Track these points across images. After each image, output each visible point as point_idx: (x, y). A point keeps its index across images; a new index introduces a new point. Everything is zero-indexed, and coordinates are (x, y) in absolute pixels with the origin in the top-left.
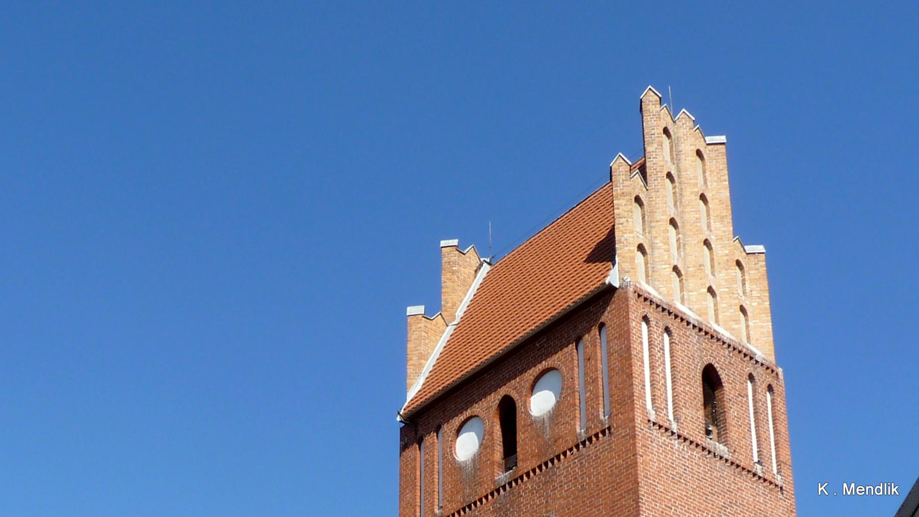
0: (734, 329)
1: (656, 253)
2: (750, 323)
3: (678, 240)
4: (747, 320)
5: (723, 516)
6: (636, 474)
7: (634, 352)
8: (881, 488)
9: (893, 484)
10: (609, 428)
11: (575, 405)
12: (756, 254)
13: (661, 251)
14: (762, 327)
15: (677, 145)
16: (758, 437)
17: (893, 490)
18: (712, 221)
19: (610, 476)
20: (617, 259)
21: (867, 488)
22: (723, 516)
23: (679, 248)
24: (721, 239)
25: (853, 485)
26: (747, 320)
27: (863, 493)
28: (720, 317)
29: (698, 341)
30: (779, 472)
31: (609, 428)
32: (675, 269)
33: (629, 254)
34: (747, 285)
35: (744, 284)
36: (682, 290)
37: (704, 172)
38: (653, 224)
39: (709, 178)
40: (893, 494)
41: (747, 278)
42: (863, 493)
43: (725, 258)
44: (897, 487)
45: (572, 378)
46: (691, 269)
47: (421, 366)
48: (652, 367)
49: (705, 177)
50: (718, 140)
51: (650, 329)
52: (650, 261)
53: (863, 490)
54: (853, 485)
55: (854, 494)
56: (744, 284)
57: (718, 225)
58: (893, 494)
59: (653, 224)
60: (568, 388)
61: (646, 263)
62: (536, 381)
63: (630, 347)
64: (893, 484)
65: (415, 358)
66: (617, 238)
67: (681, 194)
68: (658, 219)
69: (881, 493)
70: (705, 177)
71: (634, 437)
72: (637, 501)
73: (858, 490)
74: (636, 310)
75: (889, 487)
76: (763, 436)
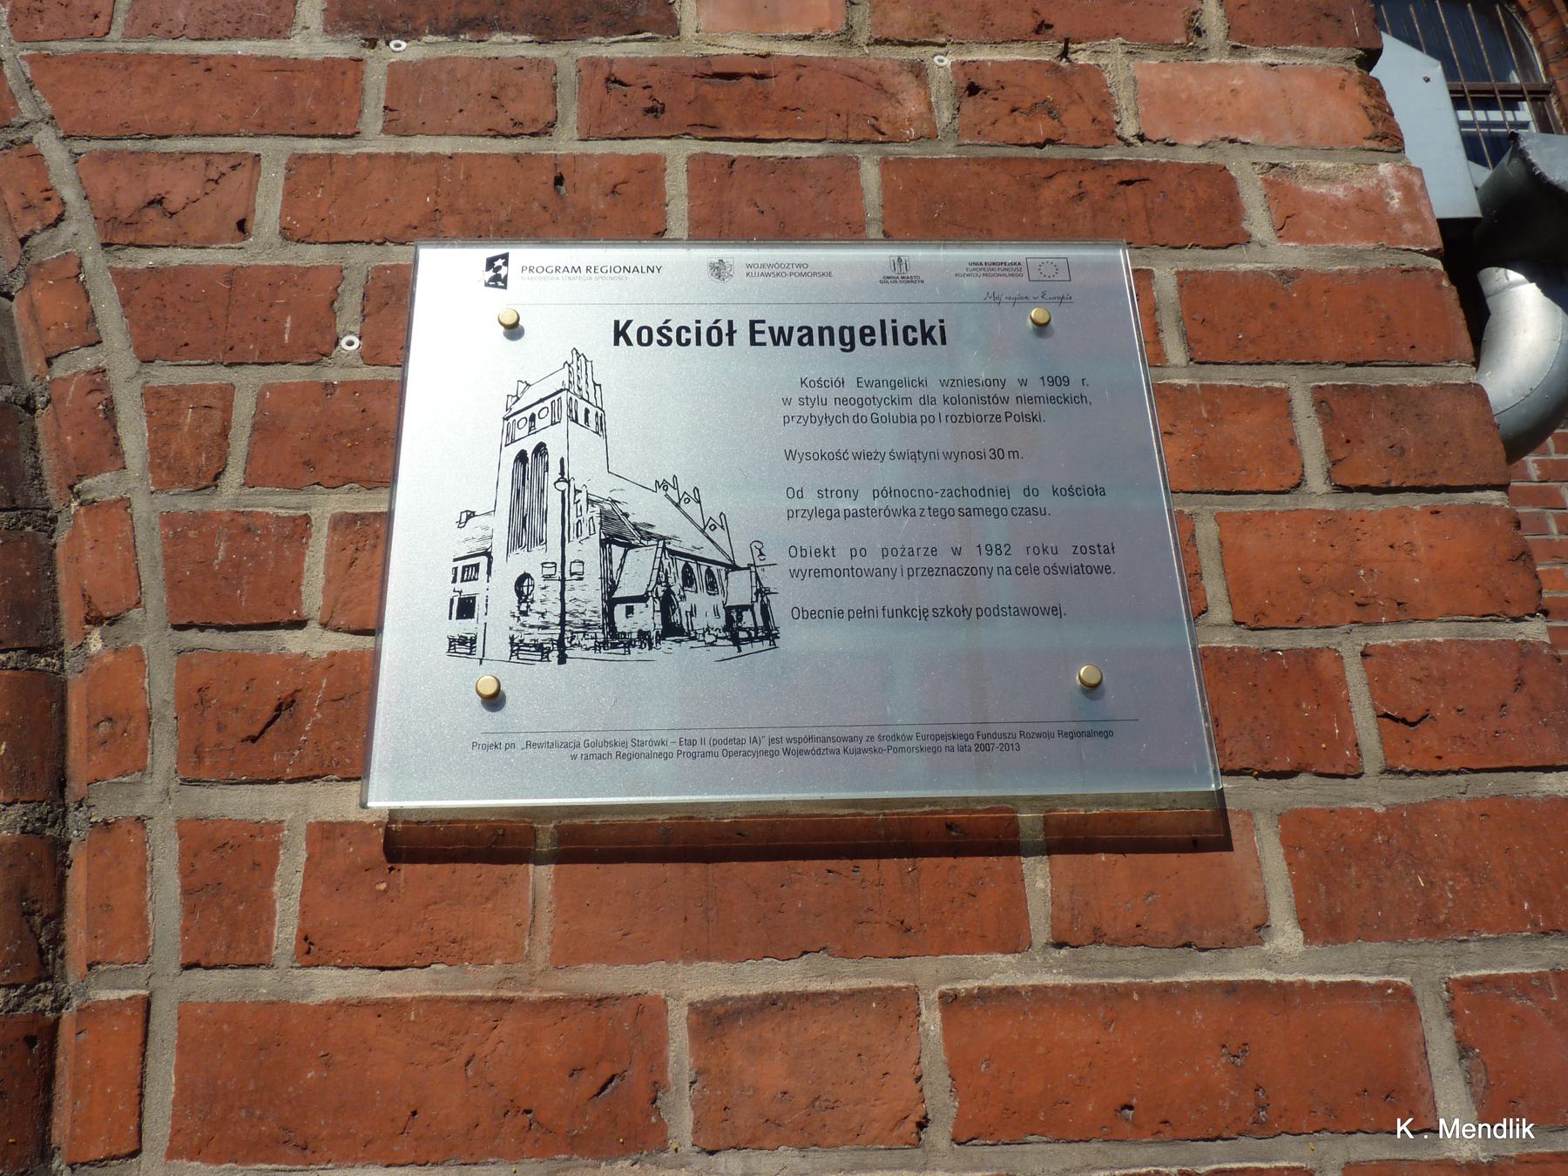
5: (263, 4)
8: (1504, 1126)
9: (1524, 1120)
12: (747, 80)
17: (1525, 1130)
21: (1481, 1126)
22: (263, 4)
25: (1457, 1121)
27: (1474, 1135)
29: (27, 148)
40: (1524, 1137)
42: (1474, 1135)
44: (1531, 1125)
45: (1462, 665)
50: (481, 149)
51: (75, 490)
53: (1474, 1130)
54: (1457, 1121)
55: (1458, 1137)
58: (1524, 1137)
63: (1226, 810)
64: (1524, 1120)
69: (1504, 1136)
73: (1464, 1131)
75: (1518, 1125)
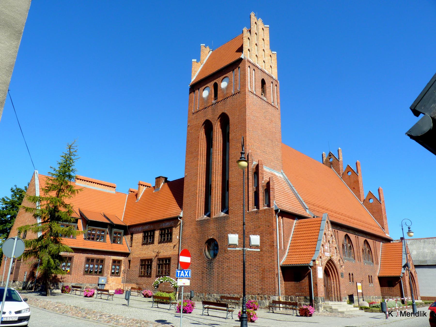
1: (252, 51)
3: (257, 49)
4: (272, 69)
7: (246, 74)
10: (240, 92)
15: (258, 26)
20: (243, 52)
23: (257, 51)
26: (272, 69)
35: (271, 61)
37: (264, 33)
48: (250, 78)
56: (271, 61)
57: (266, 46)
74: (247, 64)
76: (274, 97)
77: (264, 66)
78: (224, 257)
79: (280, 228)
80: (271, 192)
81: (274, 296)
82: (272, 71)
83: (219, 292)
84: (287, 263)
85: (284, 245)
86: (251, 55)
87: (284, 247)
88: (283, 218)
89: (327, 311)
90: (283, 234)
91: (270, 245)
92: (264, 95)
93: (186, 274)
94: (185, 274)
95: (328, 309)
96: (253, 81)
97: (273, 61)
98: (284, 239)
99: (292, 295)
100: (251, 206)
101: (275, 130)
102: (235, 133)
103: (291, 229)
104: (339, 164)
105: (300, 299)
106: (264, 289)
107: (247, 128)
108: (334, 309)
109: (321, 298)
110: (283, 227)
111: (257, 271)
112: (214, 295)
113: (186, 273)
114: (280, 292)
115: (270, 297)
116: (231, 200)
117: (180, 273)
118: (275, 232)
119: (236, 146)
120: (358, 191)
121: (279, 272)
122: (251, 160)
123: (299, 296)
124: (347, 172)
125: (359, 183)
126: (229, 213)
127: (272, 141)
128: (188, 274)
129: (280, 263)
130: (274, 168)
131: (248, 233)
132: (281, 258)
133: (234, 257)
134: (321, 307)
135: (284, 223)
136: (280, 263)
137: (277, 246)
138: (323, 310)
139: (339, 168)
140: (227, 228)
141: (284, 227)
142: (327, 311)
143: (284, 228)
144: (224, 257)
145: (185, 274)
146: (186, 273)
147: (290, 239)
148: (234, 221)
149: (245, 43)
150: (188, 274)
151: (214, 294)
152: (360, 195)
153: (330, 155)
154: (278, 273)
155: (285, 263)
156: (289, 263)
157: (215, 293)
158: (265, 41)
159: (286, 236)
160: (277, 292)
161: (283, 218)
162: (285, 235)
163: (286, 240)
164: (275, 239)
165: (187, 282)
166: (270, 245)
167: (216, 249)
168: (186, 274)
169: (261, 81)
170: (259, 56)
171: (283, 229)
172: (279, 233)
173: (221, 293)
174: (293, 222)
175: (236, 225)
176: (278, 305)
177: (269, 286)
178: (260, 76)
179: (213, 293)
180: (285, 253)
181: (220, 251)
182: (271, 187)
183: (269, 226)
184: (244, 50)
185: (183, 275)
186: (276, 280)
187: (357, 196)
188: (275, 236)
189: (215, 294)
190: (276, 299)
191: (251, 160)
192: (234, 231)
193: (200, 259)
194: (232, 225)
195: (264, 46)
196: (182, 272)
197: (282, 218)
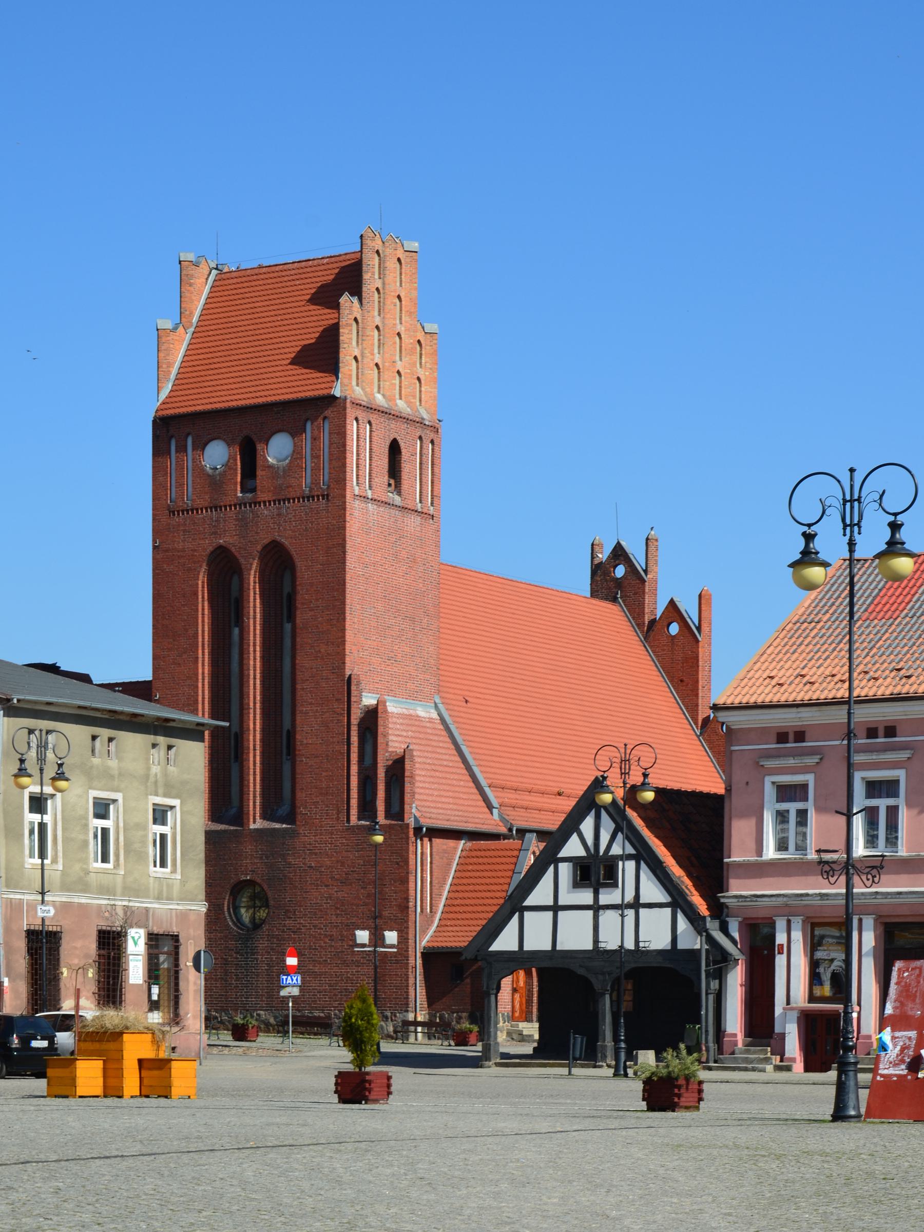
0: (411, 402)
1: (365, 360)
2: (423, 389)
3: (379, 340)
4: (420, 386)
6: (345, 535)
7: (348, 448)
10: (328, 495)
11: (302, 468)
13: (368, 360)
14: (431, 392)
15: (384, 263)
16: (421, 482)
18: (403, 315)
19: (327, 529)
20: (340, 376)
23: (379, 347)
24: (409, 330)
26: (420, 386)
28: (403, 392)
30: (432, 504)
31: (328, 495)
32: (377, 365)
33: (348, 373)
34: (423, 358)
35: (421, 357)
36: (379, 381)
37: (401, 274)
38: (364, 338)
39: (403, 280)
41: (423, 352)
43: (410, 346)
46: (387, 364)
47: (169, 372)
48: (358, 455)
49: (401, 278)
52: (360, 366)
56: (421, 357)
57: (408, 319)
59: (364, 338)
60: (298, 453)
61: (358, 368)
62: (369, 748)
65: (164, 366)
66: (341, 359)
67: (384, 303)
68: (368, 334)
70: (401, 278)
71: (345, 509)
72: (344, 552)
74: (351, 413)
76: (424, 481)
77: (398, 388)
78: (285, 926)
79: (424, 868)
80: (407, 785)
81: (405, 1014)
82: (420, 391)
83: (274, 1007)
84: (435, 944)
85: (431, 904)
86: (360, 374)
87: (431, 908)
88: (433, 839)
89: (513, 1039)
90: (431, 878)
91: (399, 906)
92: (396, 487)
93: (295, 981)
94: (292, 980)
95: (515, 1036)
96: (365, 460)
97: (428, 359)
98: (431, 890)
99: (444, 1009)
100: (354, 812)
101: (421, 585)
102: (312, 613)
103: (449, 864)
104: (644, 592)
105: (460, 1018)
106: (383, 998)
107: (347, 609)
108: (526, 1035)
109: (503, 1015)
110: (431, 863)
111: (368, 960)
112: (258, 1015)
113: (295, 979)
114: (418, 1004)
115: (395, 1016)
116: (303, 789)
117: (286, 979)
118: (412, 878)
119: (317, 649)
120: (692, 691)
121: (418, 963)
122: (356, 696)
123: (457, 1012)
124: (665, 624)
125: (698, 666)
126: (298, 823)
127: (413, 620)
128: (297, 980)
129: (420, 944)
130: (414, 696)
131: (346, 874)
132: (424, 932)
133: (311, 929)
134: (501, 1032)
135: (434, 853)
136: (420, 944)
137: (416, 906)
138: (504, 1037)
139: (642, 605)
140: (291, 859)
141: (434, 862)
142: (513, 1039)
143: (434, 866)
144: (285, 926)
145: (292, 980)
146: (295, 979)
147: (447, 887)
148: (310, 844)
149: (345, 346)
150: (297, 980)
151: (258, 1012)
152: (697, 705)
153: (619, 554)
154: (416, 965)
155: (431, 945)
156: (440, 945)
157: (261, 1010)
158: (403, 303)
159: (439, 883)
160: (412, 1005)
161: (433, 840)
162: (435, 882)
163: (435, 891)
164: (412, 892)
165: (296, 992)
166: (399, 906)
167: (259, 905)
168: (295, 981)
169: (388, 444)
170: (384, 366)
171: (431, 867)
172: (422, 877)
173: (278, 1010)
174: (456, 849)
175: (316, 854)
176: (412, 1028)
177: (394, 992)
178: (385, 432)
179: (257, 1010)
180: (432, 922)
181: (274, 912)
182: (407, 774)
183: (398, 864)
184: (341, 370)
185: (291, 982)
186: (411, 981)
187: (687, 709)
188: (412, 885)
189: (262, 1012)
190: (411, 1017)
191: (356, 696)
192: (311, 867)
193: (217, 930)
194: (305, 854)
195: (401, 319)
196: (289, 977)
197: (430, 840)
